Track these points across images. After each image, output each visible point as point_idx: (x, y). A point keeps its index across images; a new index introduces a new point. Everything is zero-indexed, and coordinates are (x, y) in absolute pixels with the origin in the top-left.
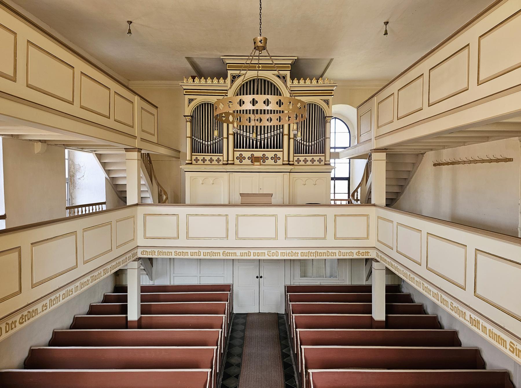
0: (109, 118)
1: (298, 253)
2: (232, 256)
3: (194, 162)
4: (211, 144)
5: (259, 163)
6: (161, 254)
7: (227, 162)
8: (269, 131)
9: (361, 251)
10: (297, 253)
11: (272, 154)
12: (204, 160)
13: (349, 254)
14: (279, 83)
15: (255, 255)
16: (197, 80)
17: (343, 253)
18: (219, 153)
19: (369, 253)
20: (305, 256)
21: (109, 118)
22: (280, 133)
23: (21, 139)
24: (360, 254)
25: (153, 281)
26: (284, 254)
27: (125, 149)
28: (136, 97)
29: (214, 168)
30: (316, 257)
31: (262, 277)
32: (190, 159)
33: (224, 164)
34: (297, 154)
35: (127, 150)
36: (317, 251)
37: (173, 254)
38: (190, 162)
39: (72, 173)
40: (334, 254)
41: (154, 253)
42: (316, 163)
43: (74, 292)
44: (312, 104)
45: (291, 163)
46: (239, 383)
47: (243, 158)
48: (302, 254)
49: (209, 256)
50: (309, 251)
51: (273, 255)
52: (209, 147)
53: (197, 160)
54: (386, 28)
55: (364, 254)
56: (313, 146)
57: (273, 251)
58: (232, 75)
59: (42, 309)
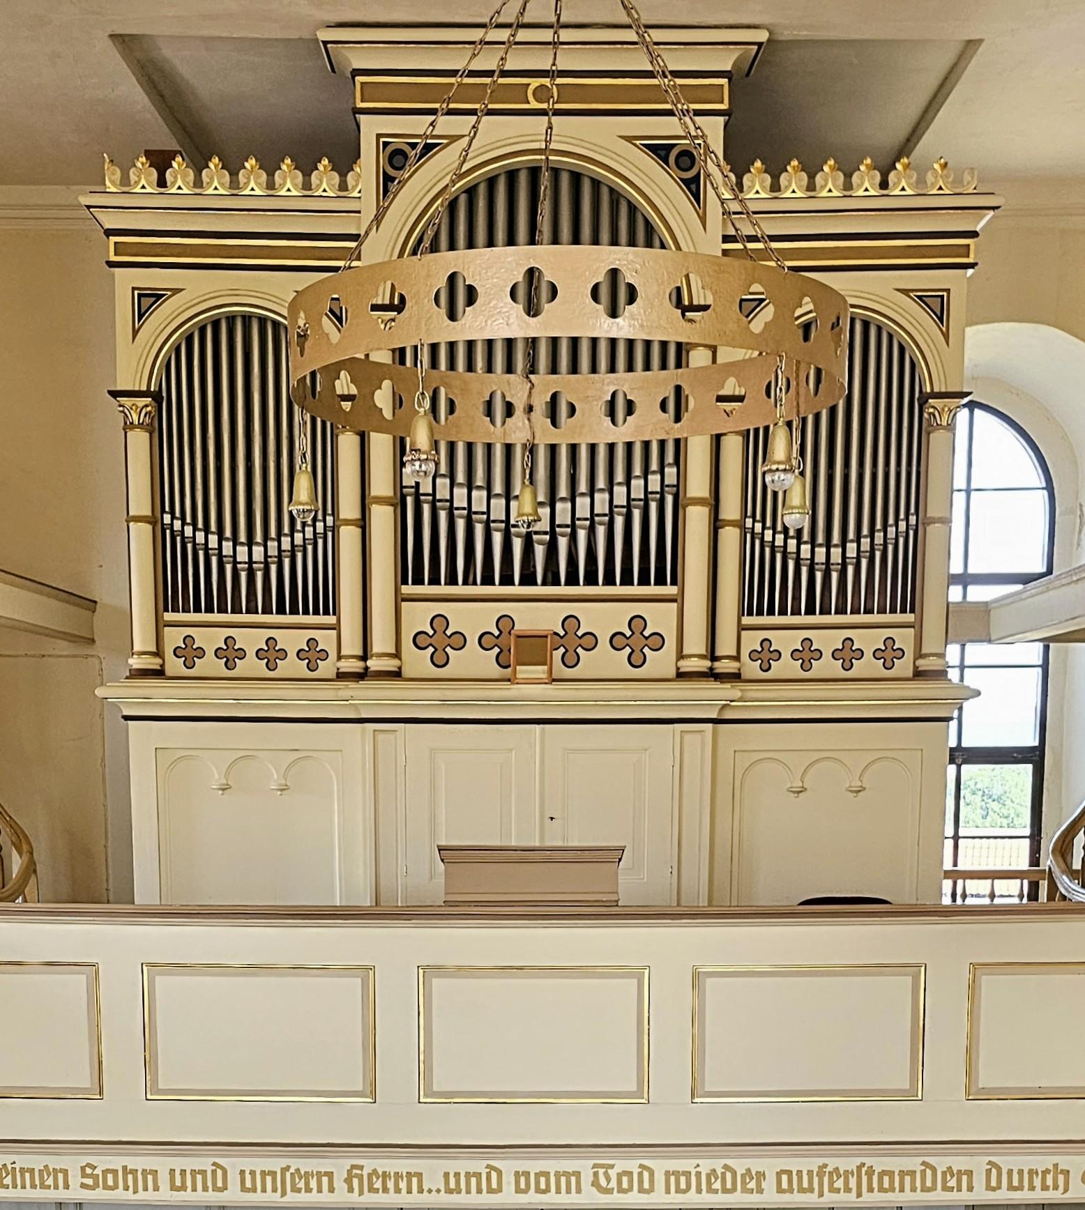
1: (761, 1176)
2: (398, 1190)
5: (545, 668)
7: (361, 664)
8: (601, 483)
15: (523, 1186)
18: (316, 612)
20: (801, 1190)
22: (662, 493)
26: (683, 1179)
30: (859, 1195)
34: (771, 612)
36: (869, 1161)
37: (75, 1179)
38: (153, 663)
40: (959, 1182)
45: (724, 666)
48: (785, 1178)
49: (275, 1190)
50: (821, 1161)
52: (259, 575)
53: (189, 653)
58: (386, 144)
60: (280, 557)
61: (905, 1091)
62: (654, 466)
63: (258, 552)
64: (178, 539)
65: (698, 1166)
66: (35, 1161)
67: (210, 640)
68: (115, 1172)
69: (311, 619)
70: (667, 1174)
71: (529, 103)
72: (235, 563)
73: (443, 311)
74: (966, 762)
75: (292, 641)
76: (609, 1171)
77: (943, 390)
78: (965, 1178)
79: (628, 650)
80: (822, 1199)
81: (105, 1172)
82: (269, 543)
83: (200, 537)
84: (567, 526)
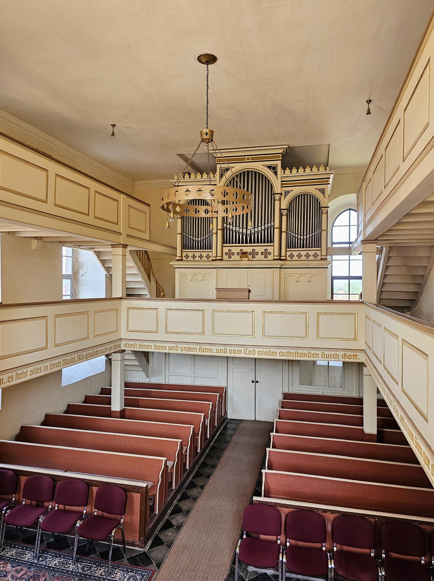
0: (88, 215)
1: (276, 352)
2: (208, 352)
3: (184, 259)
4: (201, 240)
5: (247, 258)
6: (142, 347)
7: (215, 258)
8: (260, 225)
9: (348, 354)
10: (276, 352)
11: (262, 249)
12: (194, 257)
13: (334, 356)
14: (269, 174)
15: (231, 352)
16: (193, 176)
17: (326, 355)
18: (209, 249)
19: (358, 356)
20: (284, 356)
21: (88, 215)
22: (271, 227)
23: (18, 235)
24: (346, 357)
25: (149, 379)
26: (261, 352)
27: (111, 245)
28: (122, 195)
29: (201, 264)
30: (296, 357)
31: (258, 382)
32: (181, 256)
33: (213, 260)
34: (291, 248)
35: (113, 246)
36: (298, 351)
37: (153, 347)
38: (180, 258)
39: (76, 270)
40: (316, 356)
41: (135, 346)
42: (311, 258)
43: (43, 370)
44: (307, 195)
45: (282, 258)
46: (208, 482)
47: (232, 254)
48: (281, 353)
49: (186, 351)
50: (288, 350)
51: (250, 353)
52: (199, 243)
53: (187, 257)
54: (369, 107)
55: (351, 357)
56: (308, 240)
57: (249, 349)
59: (8, 380)
60: (203, 240)
61: (265, 335)
62: (269, 222)
63: (199, 239)
64: (186, 237)
65: (264, 350)
66: (147, 344)
67: (190, 254)
68: (159, 346)
69: (208, 250)
70: (258, 351)
71: (246, 160)
72: (195, 241)
73: (223, 195)
74: (351, 279)
75: (204, 254)
76: (247, 350)
77: (277, 193)
78: (317, 355)
79: (264, 255)
80: (288, 358)
81: (158, 346)
82: (201, 237)
83: (190, 236)
84: (253, 233)
